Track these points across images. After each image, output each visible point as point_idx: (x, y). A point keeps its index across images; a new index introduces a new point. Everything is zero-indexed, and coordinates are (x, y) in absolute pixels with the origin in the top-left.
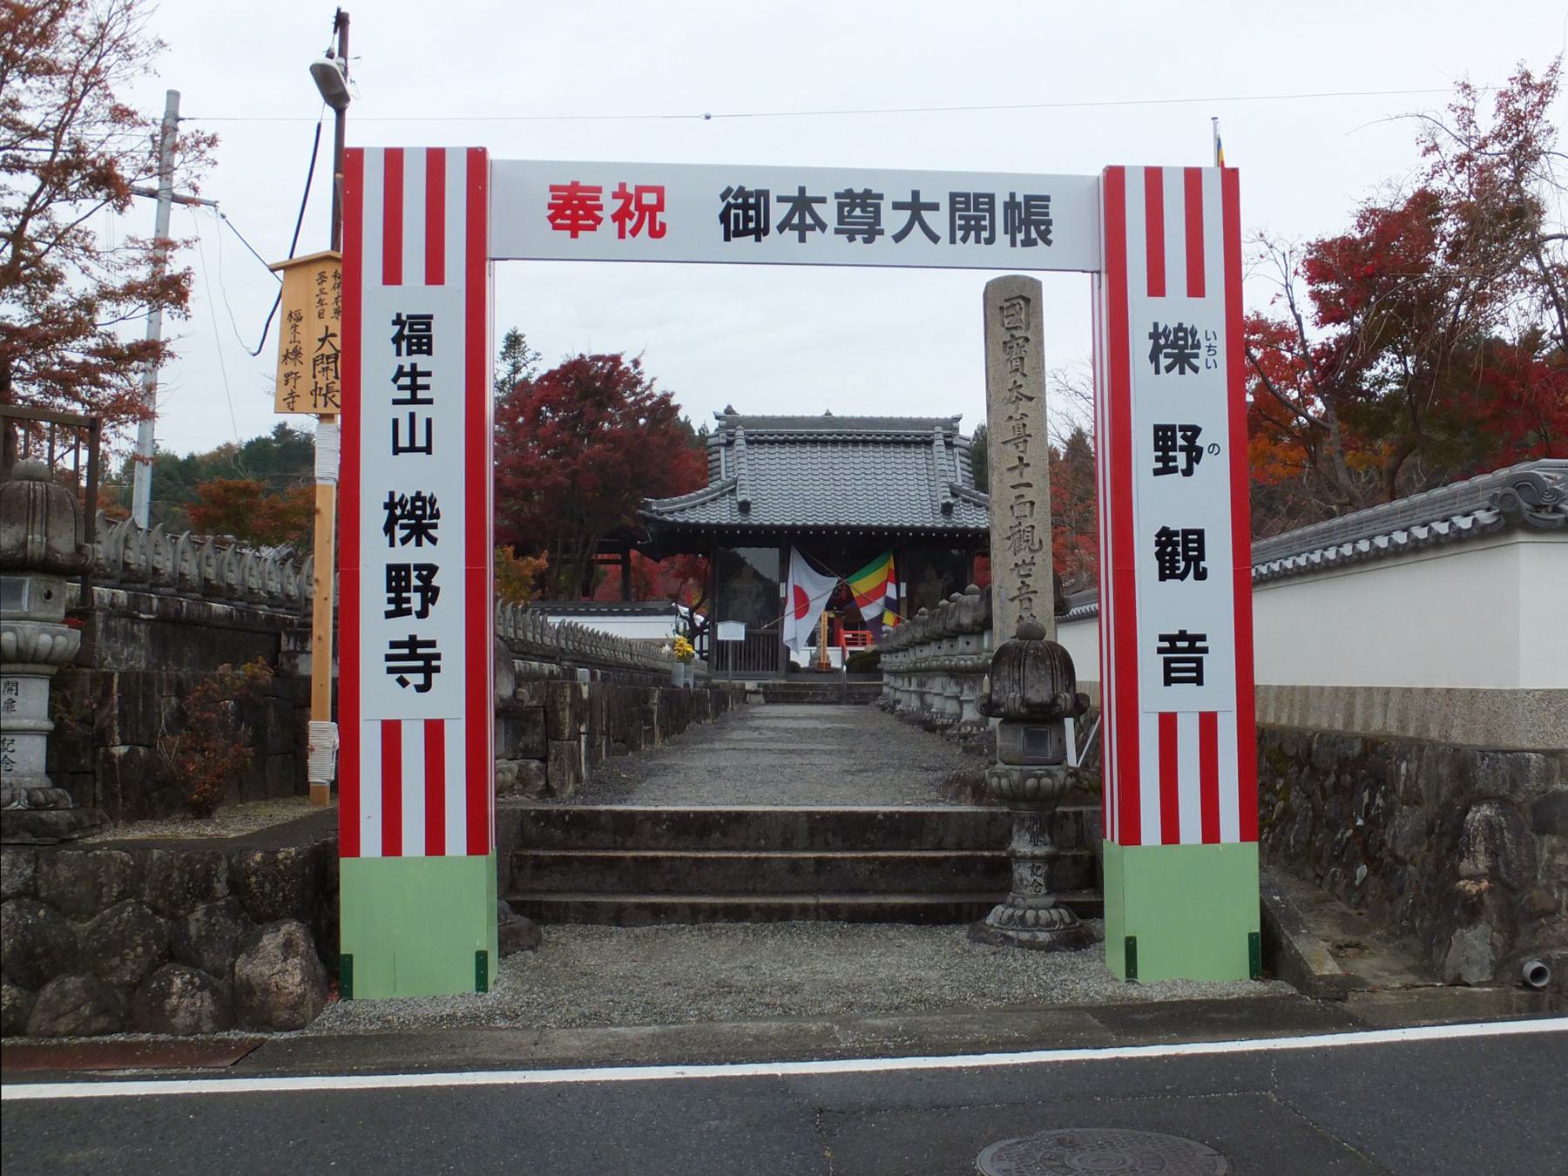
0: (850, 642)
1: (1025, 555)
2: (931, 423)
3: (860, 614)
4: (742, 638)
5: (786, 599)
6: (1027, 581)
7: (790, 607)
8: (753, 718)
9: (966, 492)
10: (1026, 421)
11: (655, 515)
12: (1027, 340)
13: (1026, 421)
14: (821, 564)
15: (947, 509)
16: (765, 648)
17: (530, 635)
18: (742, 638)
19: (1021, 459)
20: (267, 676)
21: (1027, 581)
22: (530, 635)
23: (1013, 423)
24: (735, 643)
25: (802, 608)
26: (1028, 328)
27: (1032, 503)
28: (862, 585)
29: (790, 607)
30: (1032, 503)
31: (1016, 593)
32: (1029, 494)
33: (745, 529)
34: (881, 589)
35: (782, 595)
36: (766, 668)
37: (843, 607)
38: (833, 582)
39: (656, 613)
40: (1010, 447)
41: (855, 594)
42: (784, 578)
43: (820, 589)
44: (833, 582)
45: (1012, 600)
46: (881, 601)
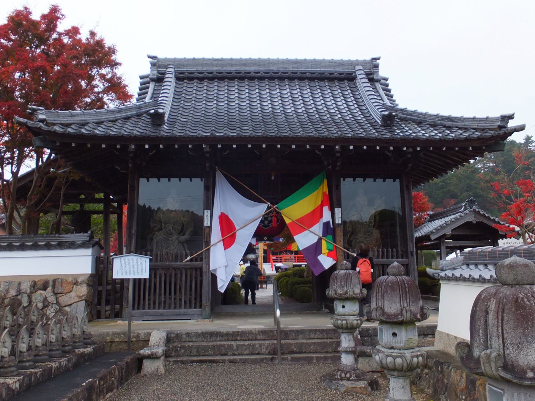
0: (276, 261)
2: (353, 64)
3: (135, 188)
4: (146, 275)
5: (210, 228)
7: (216, 235)
8: (332, 115)
14: (250, 190)
16: (181, 283)
18: (146, 275)
24: (137, 282)
25: (229, 240)
28: (294, 210)
29: (216, 235)
34: (317, 214)
35: (207, 223)
36: (189, 305)
37: (273, 231)
38: (261, 209)
39: (72, 245)
41: (288, 221)
42: (209, 205)
43: (248, 214)
44: (261, 209)
46: (318, 229)
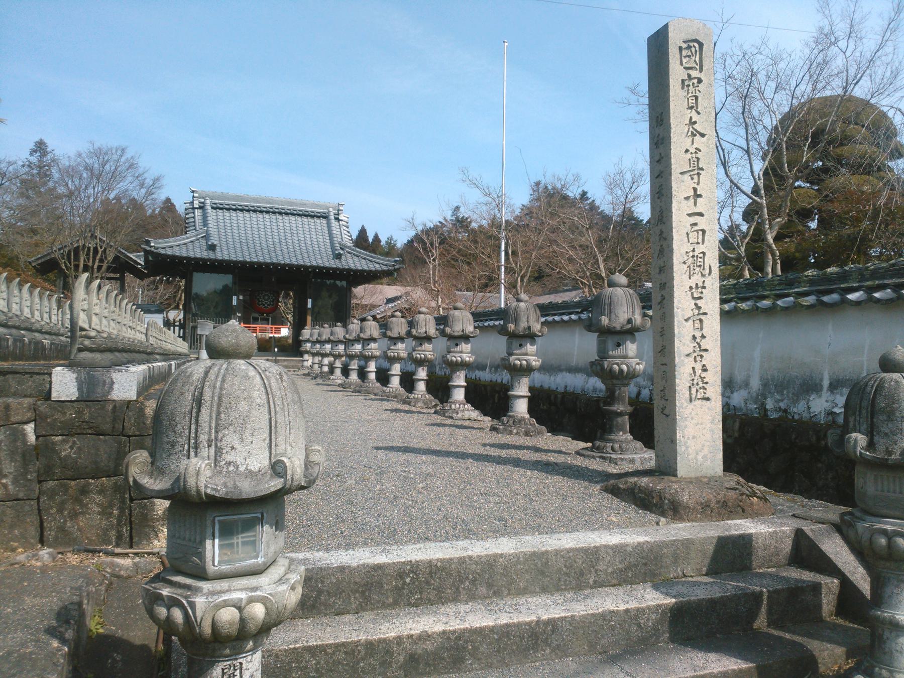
1: (697, 279)
6: (699, 302)
9: (349, 248)
10: (699, 155)
11: (153, 249)
12: (700, 81)
13: (699, 155)
15: (338, 257)
17: (27, 311)
19: (695, 190)
20: (32, 425)
21: (699, 302)
22: (27, 311)
23: (689, 156)
26: (701, 70)
27: (704, 231)
30: (704, 231)
31: (690, 314)
32: (702, 223)
33: (213, 261)
40: (686, 177)
45: (686, 320)
